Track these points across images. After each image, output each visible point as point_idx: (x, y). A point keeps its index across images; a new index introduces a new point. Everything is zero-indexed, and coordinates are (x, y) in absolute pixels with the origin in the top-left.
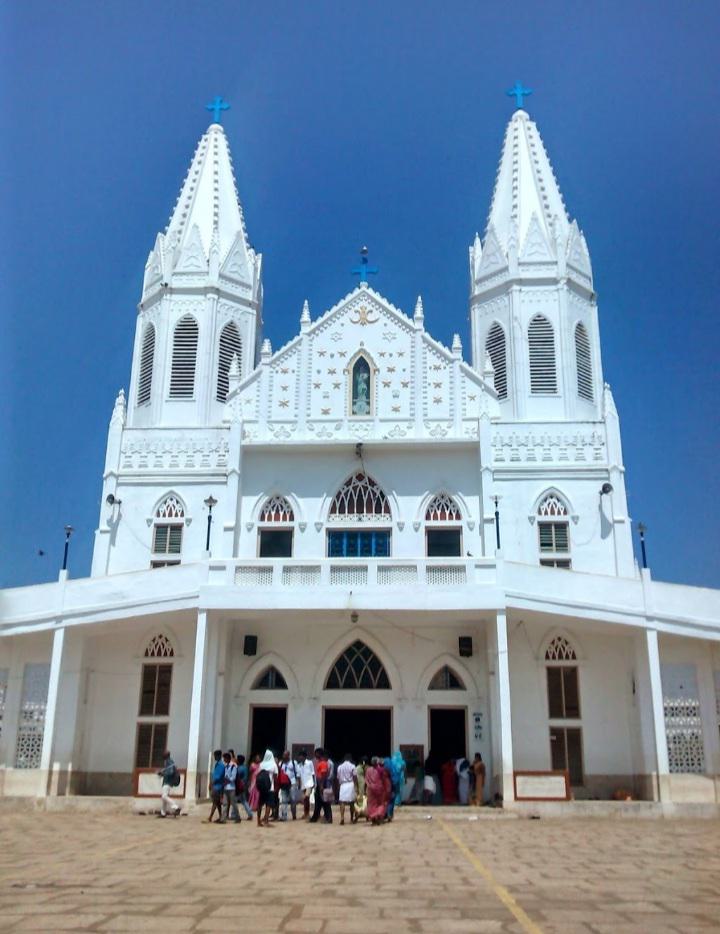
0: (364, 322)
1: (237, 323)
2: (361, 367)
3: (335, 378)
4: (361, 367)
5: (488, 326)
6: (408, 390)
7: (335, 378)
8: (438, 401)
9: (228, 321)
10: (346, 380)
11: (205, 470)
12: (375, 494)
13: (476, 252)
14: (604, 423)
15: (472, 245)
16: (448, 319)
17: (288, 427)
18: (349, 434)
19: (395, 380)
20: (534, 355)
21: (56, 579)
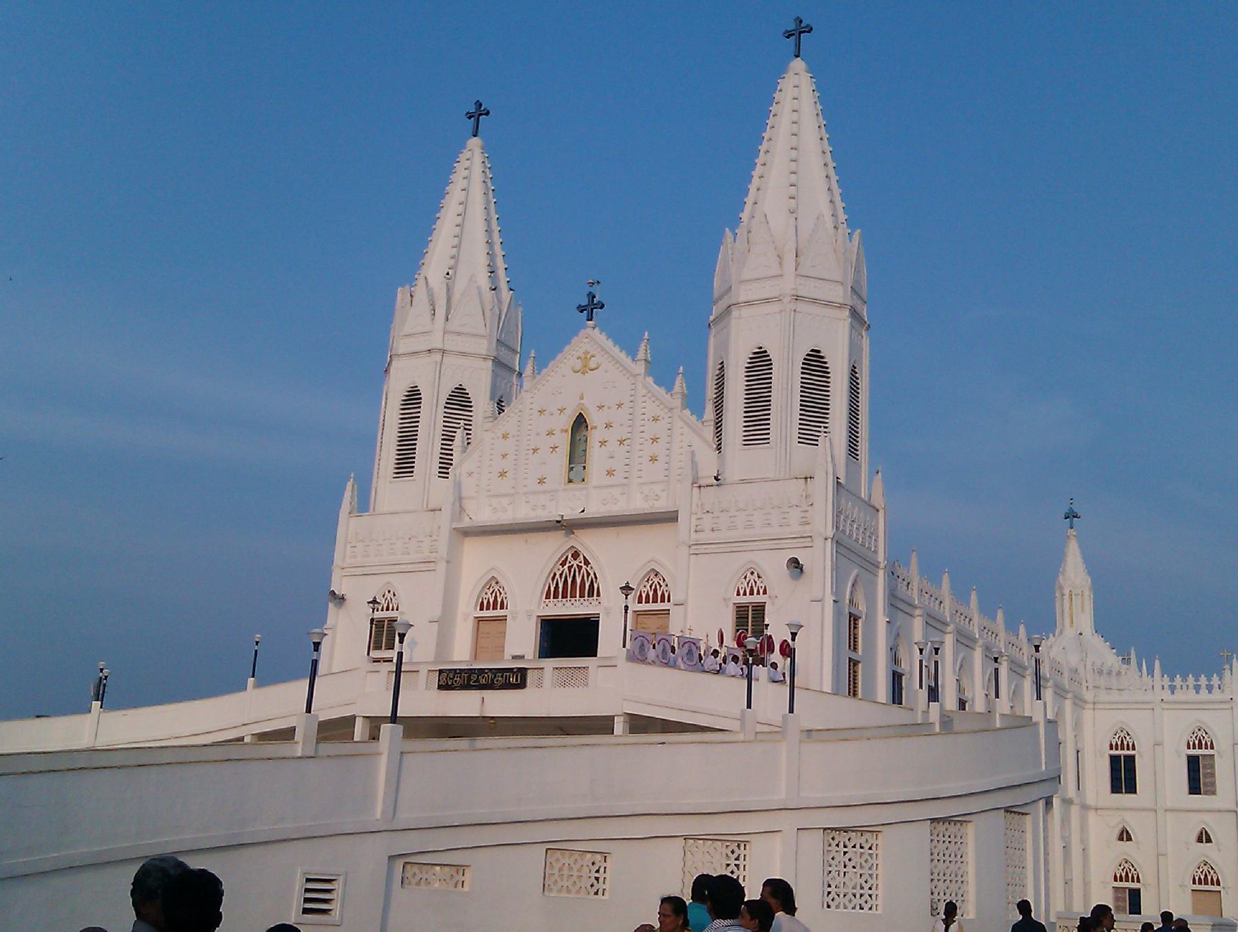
0: (585, 369)
2: (580, 422)
3: (552, 441)
6: (624, 448)
7: (552, 441)
8: (653, 459)
10: (564, 441)
11: (406, 559)
12: (588, 574)
14: (1158, 855)
17: (505, 501)
19: (612, 436)
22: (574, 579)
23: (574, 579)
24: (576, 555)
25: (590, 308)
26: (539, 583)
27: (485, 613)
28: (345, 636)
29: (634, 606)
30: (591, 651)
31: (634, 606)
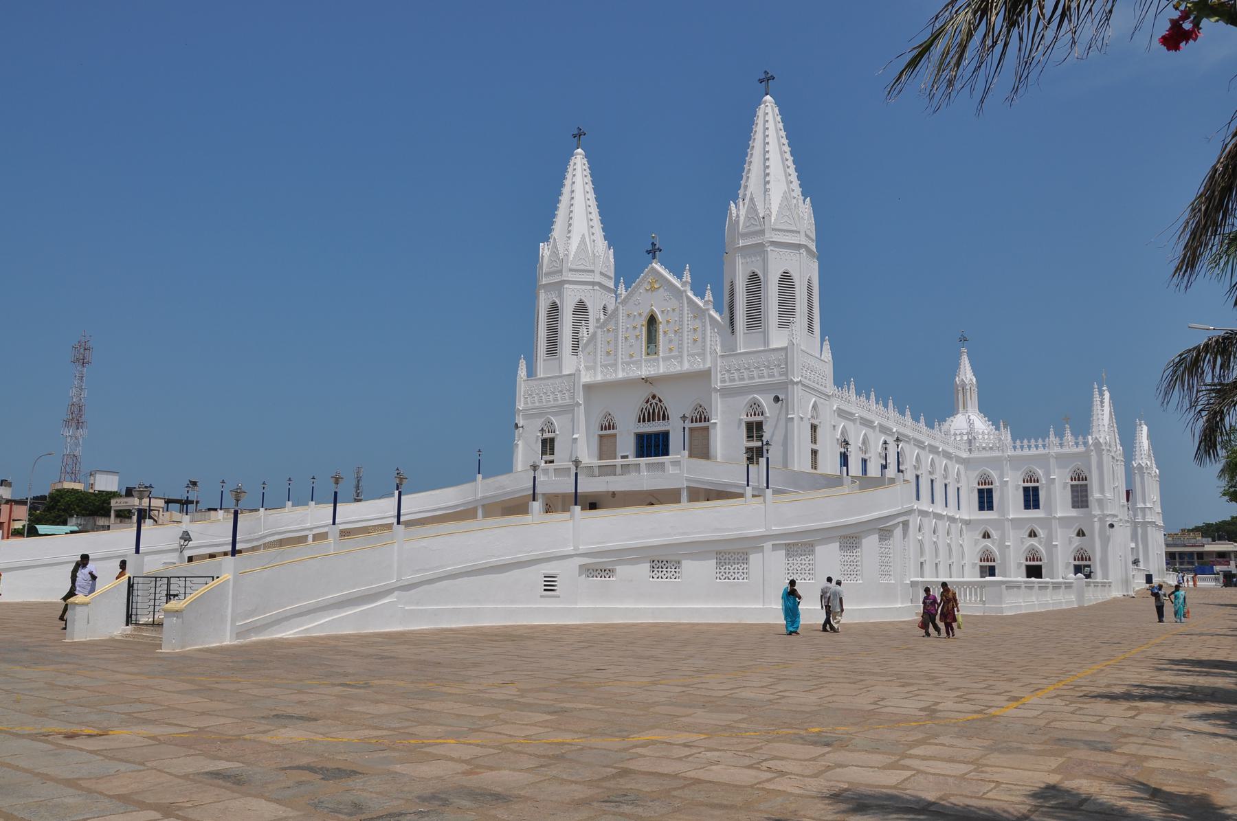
0: (652, 289)
1: (584, 299)
2: (652, 321)
4: (652, 321)
5: (549, 302)
9: (577, 299)
13: (545, 250)
15: (546, 239)
16: (709, 274)
18: (645, 371)
20: (781, 295)
21: (475, 480)
22: (653, 411)
23: (653, 411)
24: (654, 397)
25: (653, 252)
26: (635, 414)
27: (604, 432)
28: (525, 450)
29: (688, 425)
30: (666, 452)
31: (688, 425)
